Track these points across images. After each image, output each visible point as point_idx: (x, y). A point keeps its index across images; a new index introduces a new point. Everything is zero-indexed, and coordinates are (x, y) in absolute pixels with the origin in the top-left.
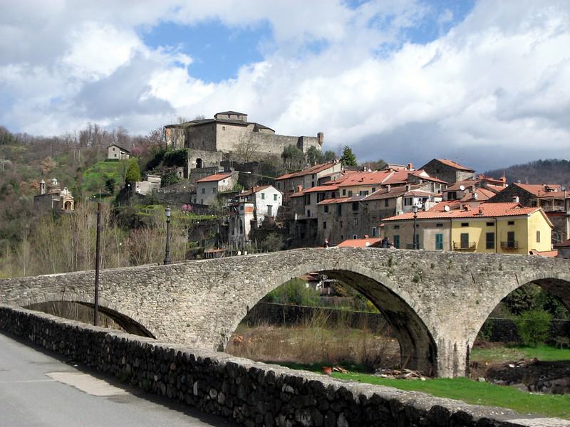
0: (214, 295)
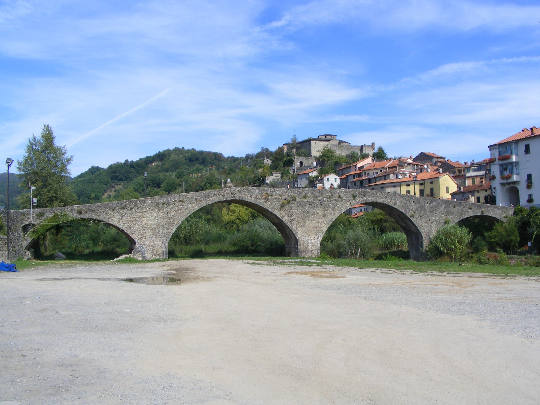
0: (161, 214)
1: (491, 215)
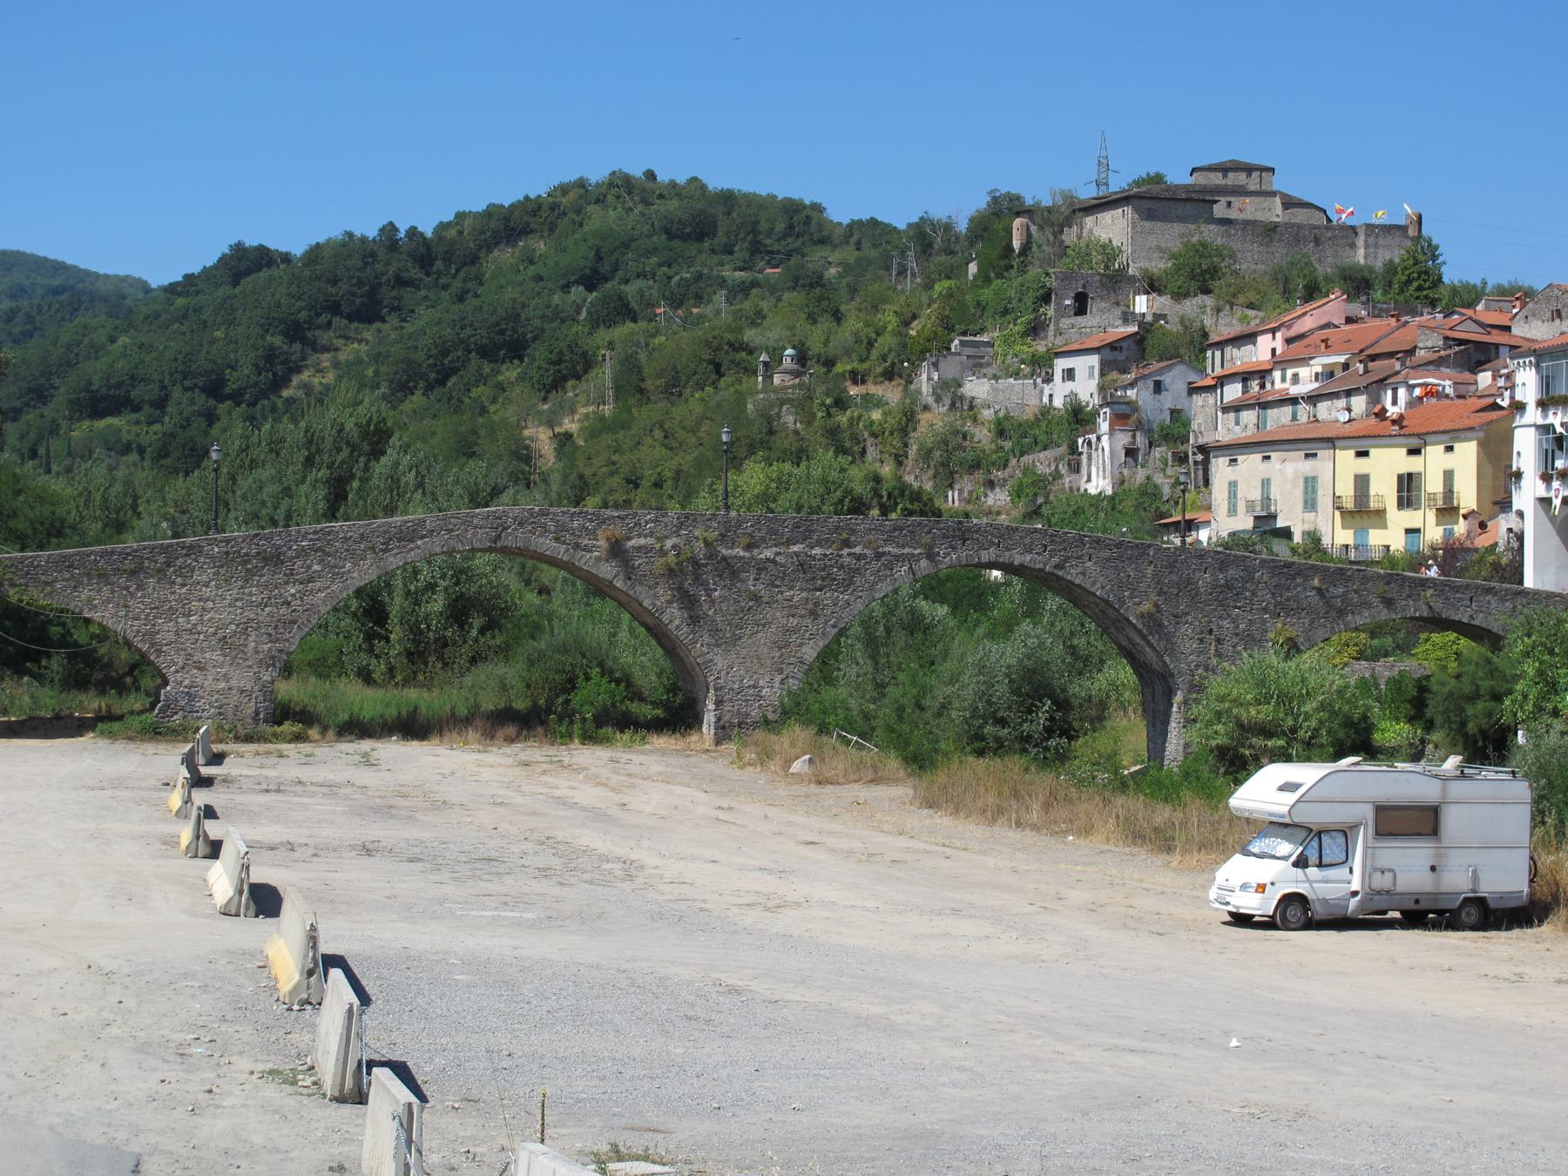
1: (1465, 620)
